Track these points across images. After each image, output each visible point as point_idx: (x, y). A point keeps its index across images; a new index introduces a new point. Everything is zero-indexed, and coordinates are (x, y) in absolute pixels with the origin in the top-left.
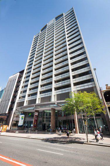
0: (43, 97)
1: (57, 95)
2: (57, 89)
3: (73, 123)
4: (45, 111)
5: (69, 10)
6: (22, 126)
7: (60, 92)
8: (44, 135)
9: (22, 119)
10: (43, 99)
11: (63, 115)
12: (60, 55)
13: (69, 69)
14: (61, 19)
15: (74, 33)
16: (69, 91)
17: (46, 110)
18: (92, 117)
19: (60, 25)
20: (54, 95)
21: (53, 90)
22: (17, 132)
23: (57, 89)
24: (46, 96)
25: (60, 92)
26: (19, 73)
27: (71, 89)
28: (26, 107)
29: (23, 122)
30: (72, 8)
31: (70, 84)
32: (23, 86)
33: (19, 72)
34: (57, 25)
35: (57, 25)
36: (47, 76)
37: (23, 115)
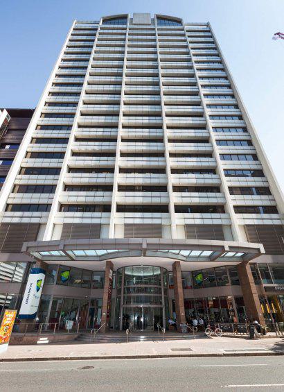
0: (134, 225)
1: (126, 225)
2: (64, 207)
4: (128, 273)
5: (85, 21)
6: (33, 316)
7: (76, 218)
9: (38, 291)
10: (71, 231)
13: (114, 165)
14: (117, 29)
17: (132, 267)
18: (94, 294)
19: (145, 43)
20: (54, 225)
21: (55, 207)
23: (64, 207)
24: (25, 220)
25: (76, 218)
28: (51, 246)
29: (37, 302)
32: (29, 150)
36: (195, 164)
37: (41, 276)
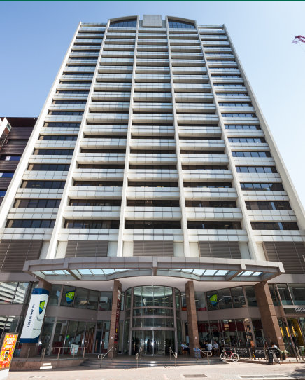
2: (68, 223)
3: (295, 331)
6: (36, 340)
7: (82, 234)
8: (127, 371)
10: (76, 248)
11: (170, 308)
12: (151, 131)
15: (84, 79)
16: (111, 238)
20: (58, 242)
21: (59, 223)
22: (47, 365)
25: (82, 234)
26: (6, 122)
27: (118, 234)
28: (55, 264)
30: (294, 42)
31: (119, 221)
33: (8, 119)
34: (113, 40)
35: (113, 40)
37: (44, 297)
